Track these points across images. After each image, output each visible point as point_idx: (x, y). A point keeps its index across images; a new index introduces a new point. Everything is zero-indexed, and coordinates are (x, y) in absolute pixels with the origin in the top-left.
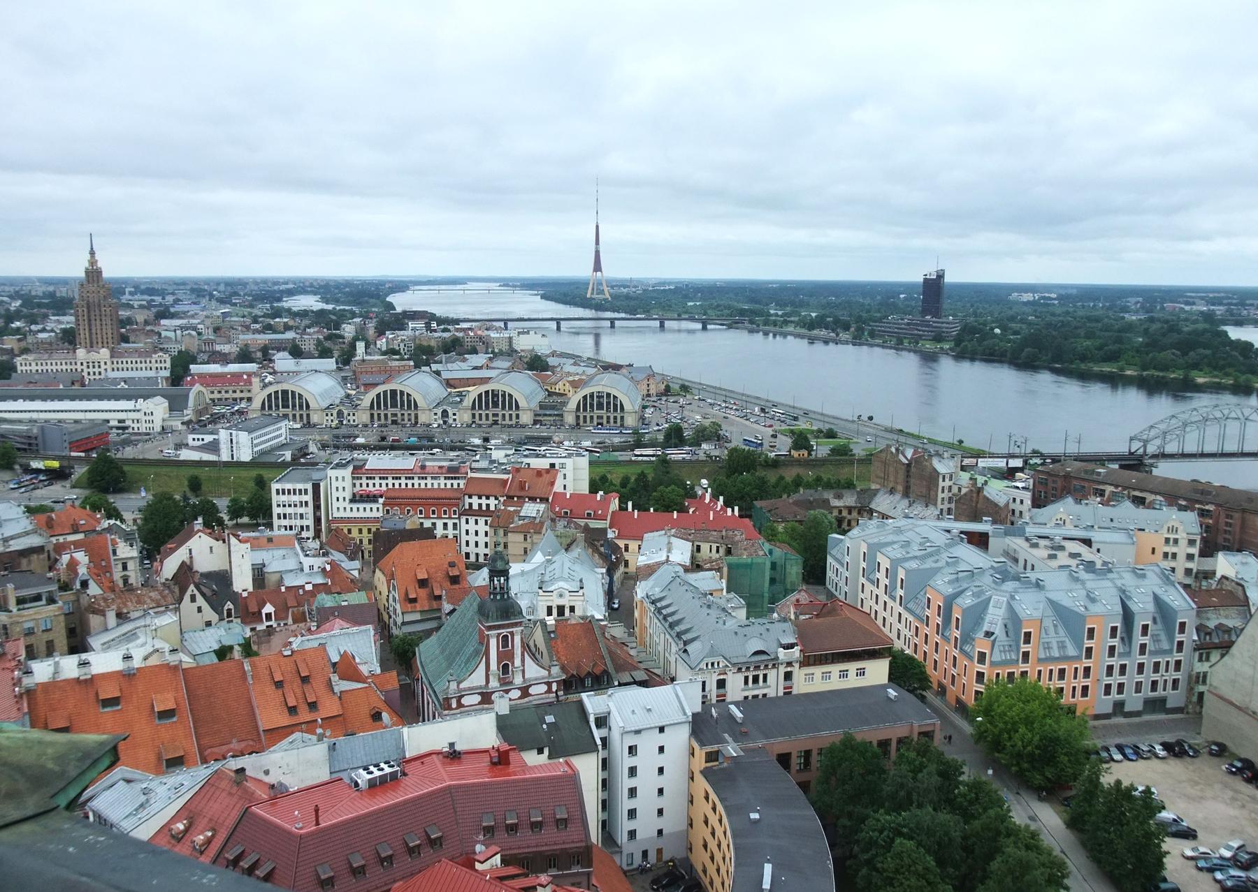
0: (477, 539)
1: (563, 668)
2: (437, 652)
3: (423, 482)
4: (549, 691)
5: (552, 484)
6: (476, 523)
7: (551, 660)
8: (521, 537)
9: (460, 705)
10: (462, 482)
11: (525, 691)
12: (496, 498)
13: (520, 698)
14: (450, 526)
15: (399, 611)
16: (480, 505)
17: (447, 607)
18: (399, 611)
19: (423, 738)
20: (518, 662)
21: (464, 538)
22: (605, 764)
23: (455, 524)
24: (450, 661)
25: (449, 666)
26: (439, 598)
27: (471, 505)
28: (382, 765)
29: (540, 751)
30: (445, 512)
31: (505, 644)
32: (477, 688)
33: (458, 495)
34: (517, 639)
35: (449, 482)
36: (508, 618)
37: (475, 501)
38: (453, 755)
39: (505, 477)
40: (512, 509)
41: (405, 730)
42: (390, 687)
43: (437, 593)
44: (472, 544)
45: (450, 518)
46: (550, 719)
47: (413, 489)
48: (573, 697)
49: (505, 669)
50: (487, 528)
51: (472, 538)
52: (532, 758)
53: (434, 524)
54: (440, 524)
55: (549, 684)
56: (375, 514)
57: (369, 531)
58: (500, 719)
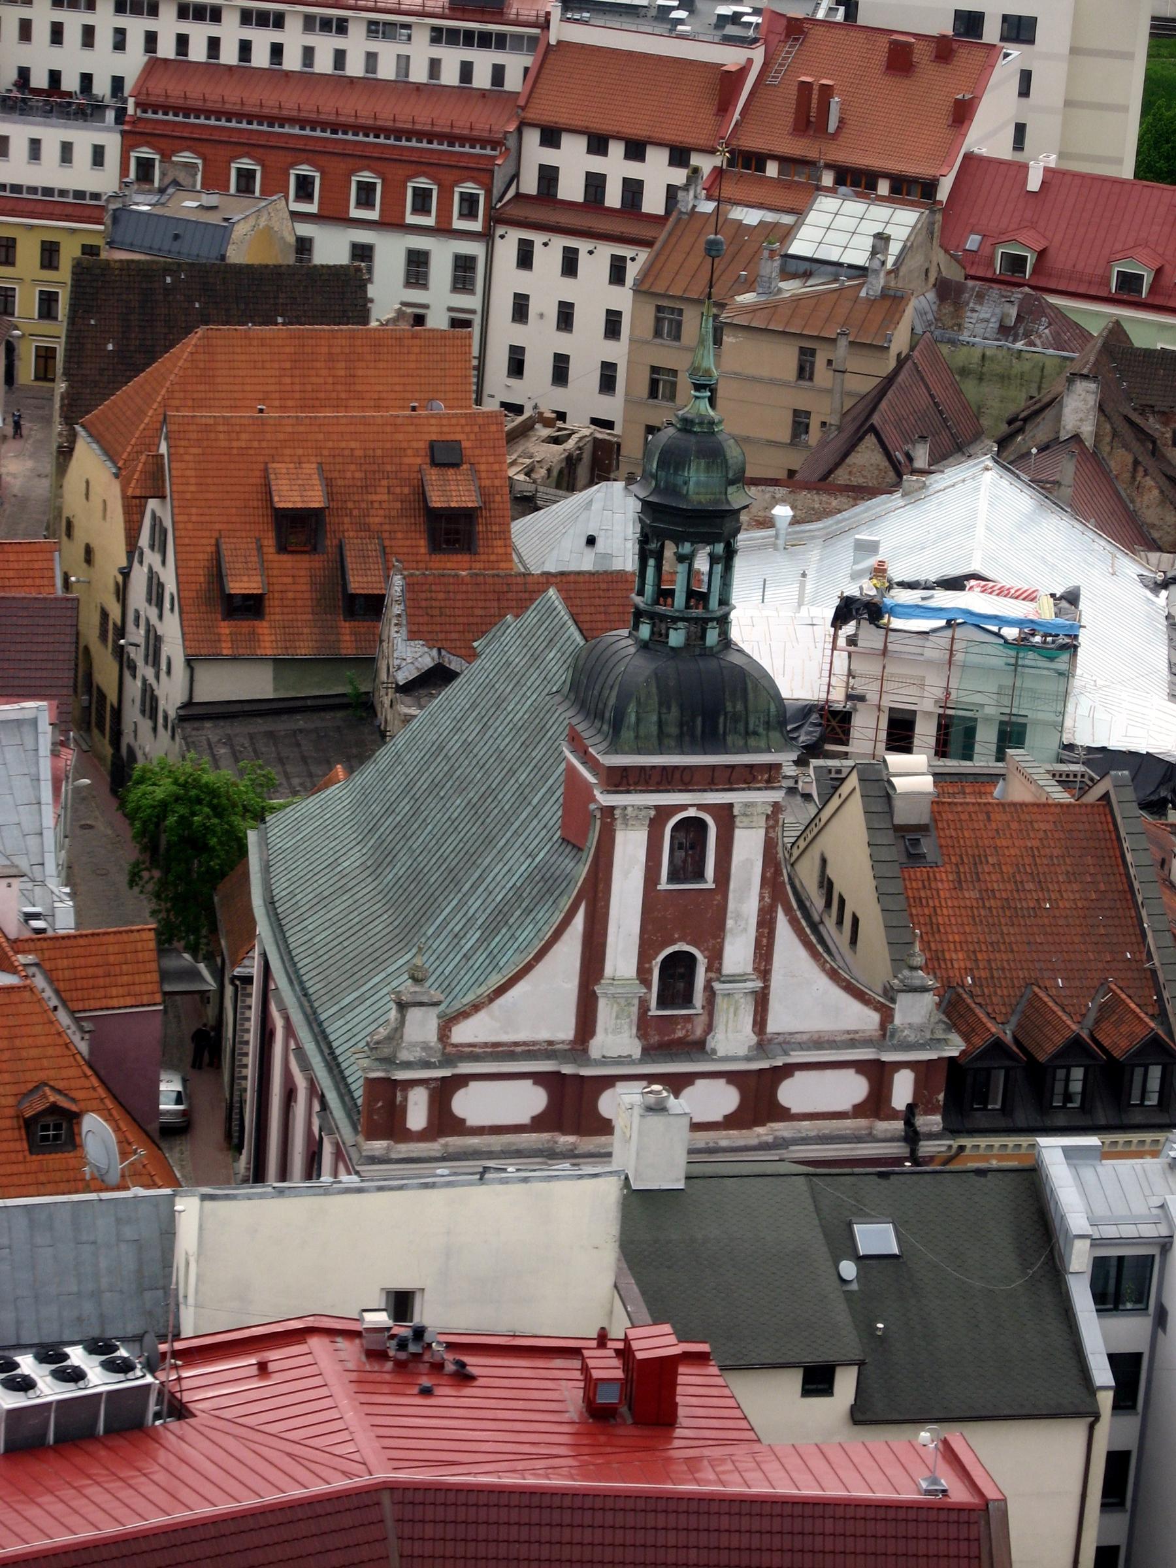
0: (563, 343)
1: (954, 1010)
2: (352, 861)
3: (325, 45)
4: (876, 1103)
5: (962, 113)
6: (570, 266)
7: (900, 962)
8: (786, 359)
9: (444, 1122)
10: (516, 64)
11: (759, 1096)
12: (679, 157)
13: (731, 1122)
14: (441, 270)
15: (173, 648)
16: (595, 183)
17: (407, 655)
18: (173, 648)
19: (256, 1250)
20: (738, 953)
21: (504, 332)
22: (1120, 1479)
23: (464, 267)
24: (413, 908)
25: (408, 932)
26: (371, 607)
27: (549, 176)
28: (77, 1356)
29: (818, 1381)
30: (422, 202)
31: (688, 860)
32: (530, 1051)
33: (483, 120)
34: (748, 847)
35: (452, 58)
36: (711, 740)
37: (573, 162)
38: (405, 1353)
39: (730, 57)
40: (751, 217)
41: (188, 1208)
42: (119, 1003)
43: (359, 583)
44: (539, 366)
45: (443, 230)
46: (876, 1237)
47: (276, 75)
48: (990, 1149)
49: (676, 979)
50: (622, 299)
51: (541, 340)
52: (773, 1404)
53: (362, 252)
54: (390, 253)
55: (878, 1075)
56: (80, 176)
57: (49, 254)
58: (642, 1208)
